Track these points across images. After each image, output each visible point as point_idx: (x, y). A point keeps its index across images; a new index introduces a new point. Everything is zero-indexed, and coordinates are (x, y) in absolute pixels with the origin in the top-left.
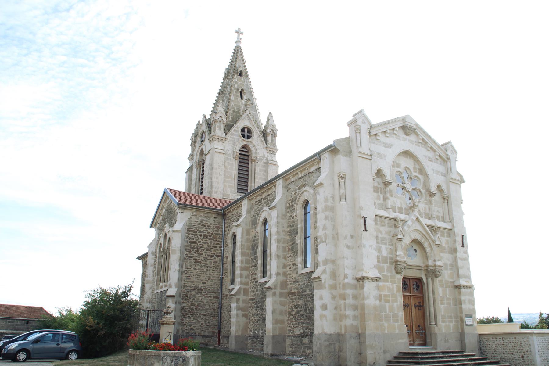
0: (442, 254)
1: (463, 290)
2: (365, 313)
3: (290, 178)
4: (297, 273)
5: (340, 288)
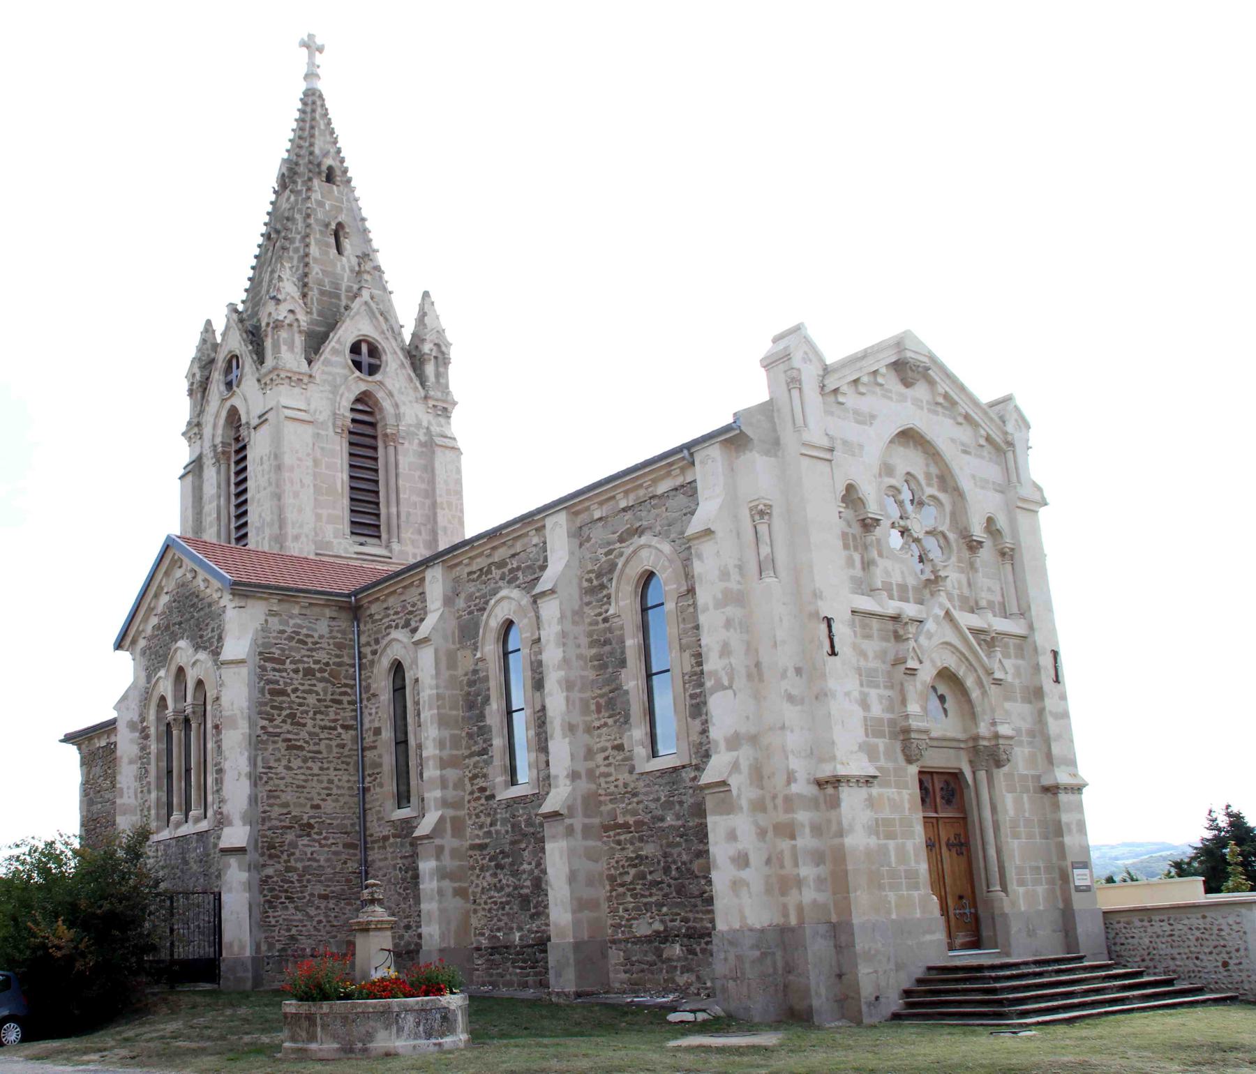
0: (1007, 705)
1: (1063, 797)
2: (846, 872)
3: (587, 509)
4: (631, 772)
5: (775, 807)
